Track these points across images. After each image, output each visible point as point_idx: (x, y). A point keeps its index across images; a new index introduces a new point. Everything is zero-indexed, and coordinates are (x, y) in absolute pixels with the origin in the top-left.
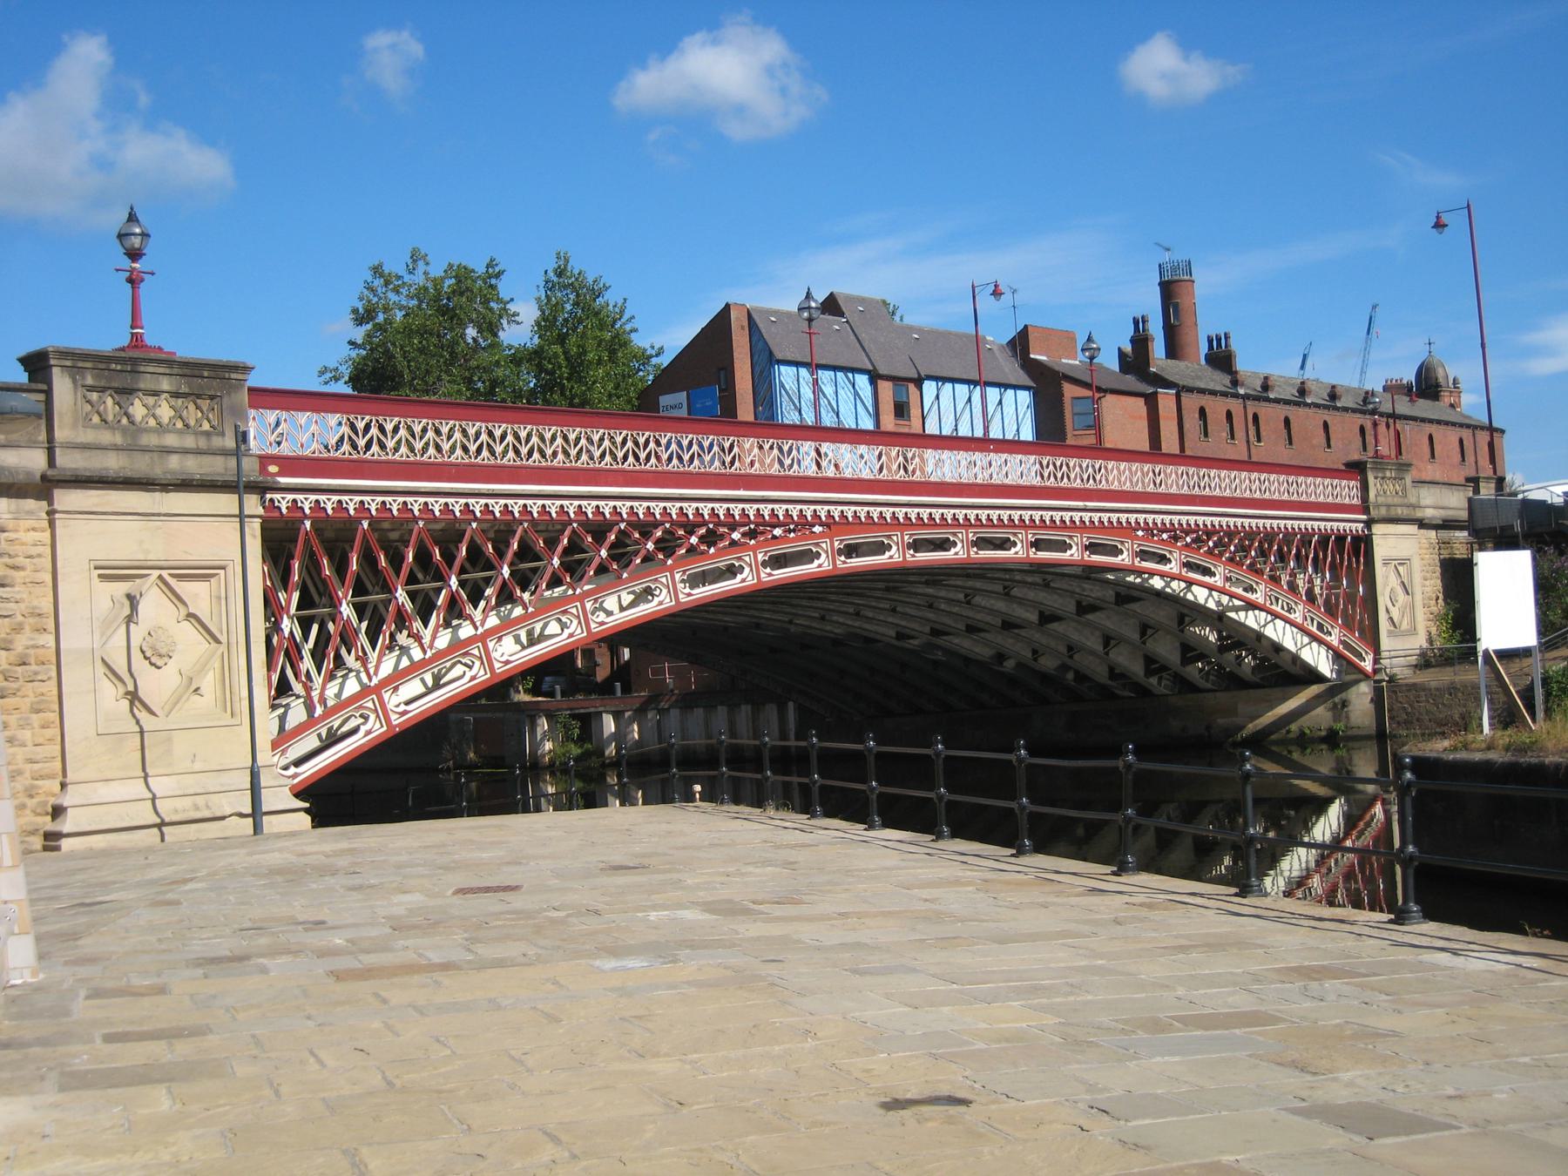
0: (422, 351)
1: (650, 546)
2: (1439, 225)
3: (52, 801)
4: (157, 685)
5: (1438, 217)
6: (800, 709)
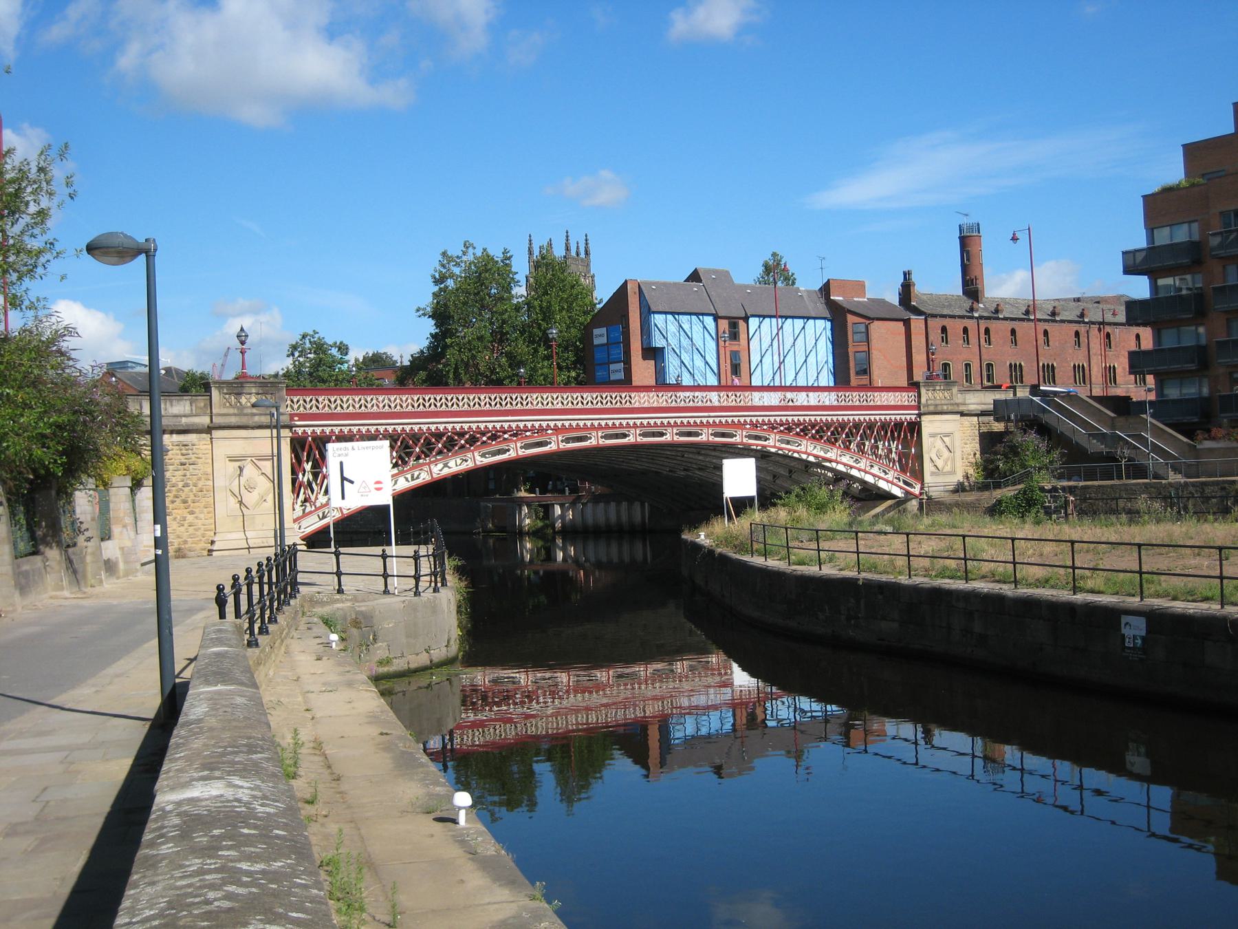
0: (465, 303)
1: (463, 442)
2: (1014, 239)
3: (211, 539)
4: (250, 498)
5: (1014, 234)
6: (650, 505)
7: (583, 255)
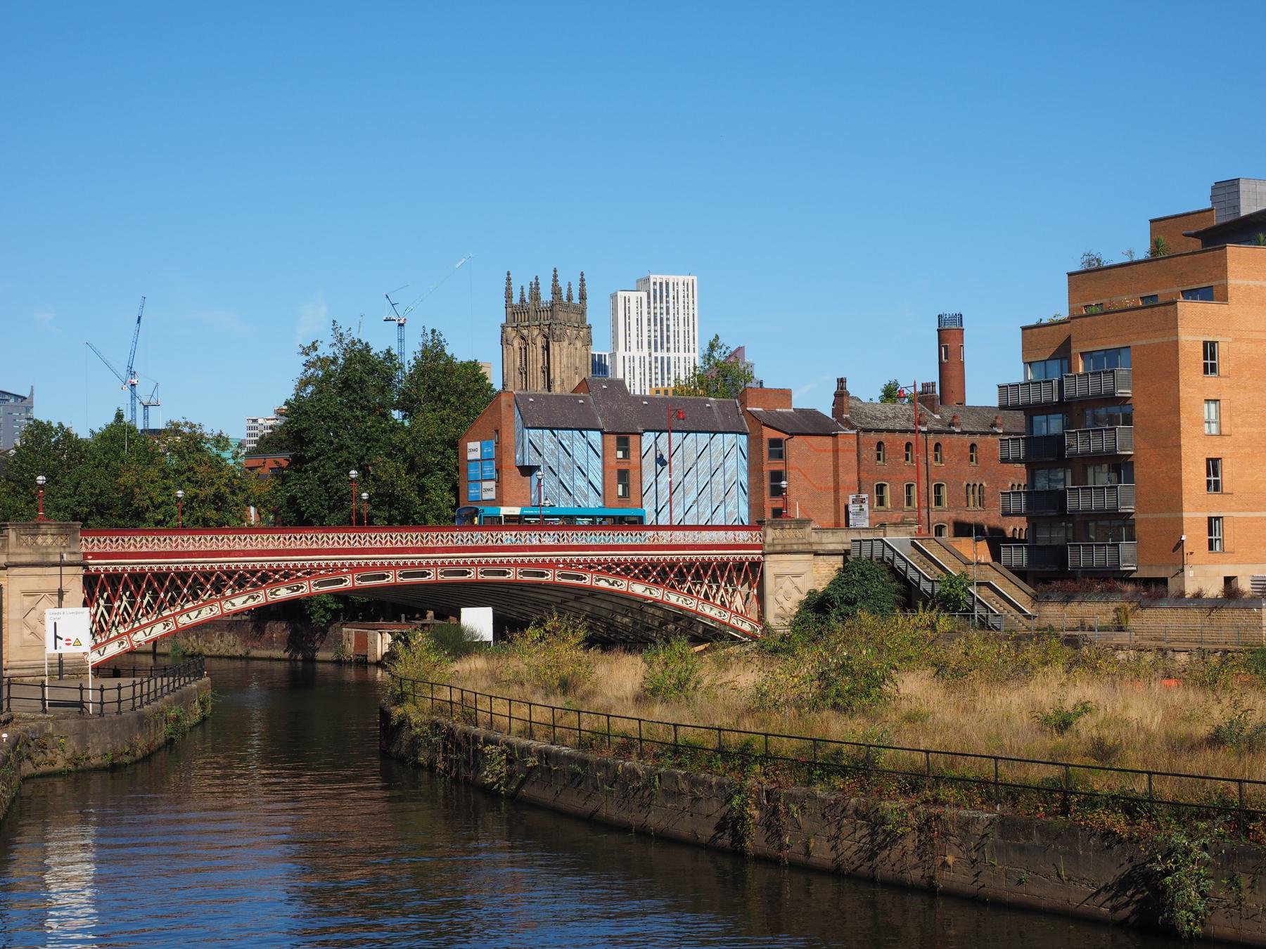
7: (576, 300)
